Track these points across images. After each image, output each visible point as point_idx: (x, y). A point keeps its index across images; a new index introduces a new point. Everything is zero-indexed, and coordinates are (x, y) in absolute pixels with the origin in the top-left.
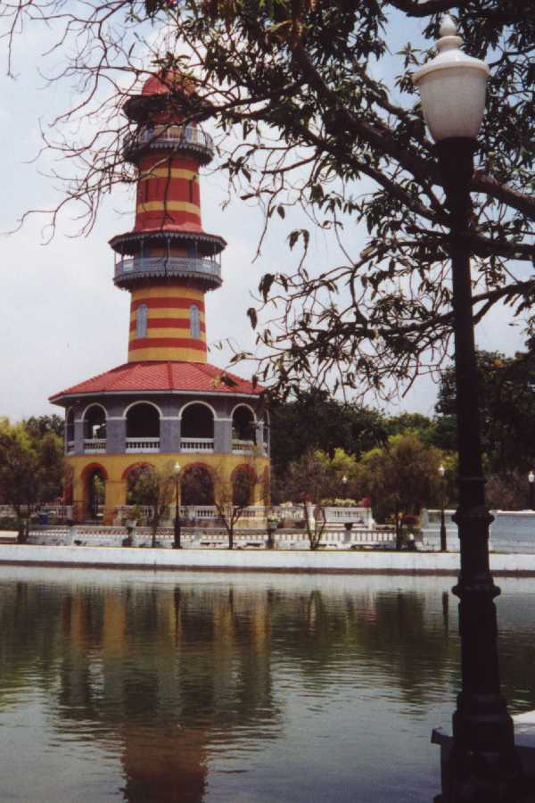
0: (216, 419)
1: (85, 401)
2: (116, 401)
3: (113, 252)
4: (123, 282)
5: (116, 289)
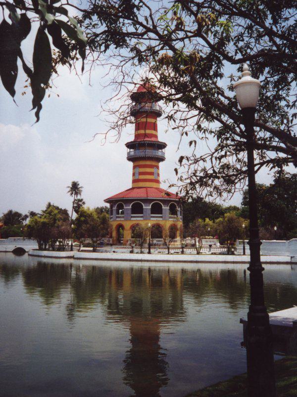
0: (163, 208)
1: (117, 201)
2: (128, 201)
3: (126, 148)
4: (130, 159)
5: (128, 161)
